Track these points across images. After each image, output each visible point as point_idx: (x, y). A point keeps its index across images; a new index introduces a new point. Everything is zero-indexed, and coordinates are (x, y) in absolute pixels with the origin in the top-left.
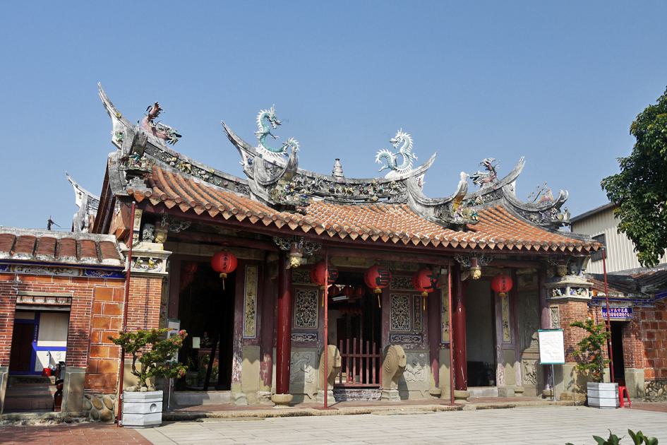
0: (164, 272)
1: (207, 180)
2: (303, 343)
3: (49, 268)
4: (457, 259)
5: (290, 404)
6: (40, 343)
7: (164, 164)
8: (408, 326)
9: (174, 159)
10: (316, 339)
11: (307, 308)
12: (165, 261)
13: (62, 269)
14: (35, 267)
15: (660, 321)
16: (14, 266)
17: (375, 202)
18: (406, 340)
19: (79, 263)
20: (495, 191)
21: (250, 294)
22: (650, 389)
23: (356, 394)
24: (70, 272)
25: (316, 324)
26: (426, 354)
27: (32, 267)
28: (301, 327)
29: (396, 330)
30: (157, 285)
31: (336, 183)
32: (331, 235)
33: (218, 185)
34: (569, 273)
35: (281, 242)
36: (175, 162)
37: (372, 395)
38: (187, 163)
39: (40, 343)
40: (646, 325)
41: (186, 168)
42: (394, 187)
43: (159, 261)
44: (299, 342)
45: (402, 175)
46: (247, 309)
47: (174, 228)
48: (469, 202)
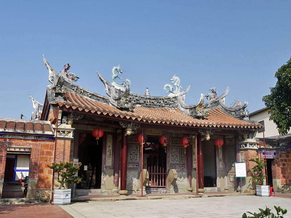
0: (71, 137)
1: (90, 97)
2: (132, 168)
3: (21, 136)
7: (71, 90)
9: (76, 88)
10: (138, 167)
11: (134, 153)
12: (72, 133)
16: (6, 135)
17: (164, 107)
19: (34, 133)
20: (216, 102)
21: (109, 147)
22: (284, 188)
27: (14, 135)
29: (173, 162)
30: (68, 143)
34: (248, 138)
35: (123, 124)
36: (76, 89)
38: (81, 90)
40: (282, 160)
41: (81, 92)
42: (172, 100)
43: (70, 132)
44: (130, 168)
45: (175, 95)
46: (108, 153)
47: (76, 118)
48: (204, 107)
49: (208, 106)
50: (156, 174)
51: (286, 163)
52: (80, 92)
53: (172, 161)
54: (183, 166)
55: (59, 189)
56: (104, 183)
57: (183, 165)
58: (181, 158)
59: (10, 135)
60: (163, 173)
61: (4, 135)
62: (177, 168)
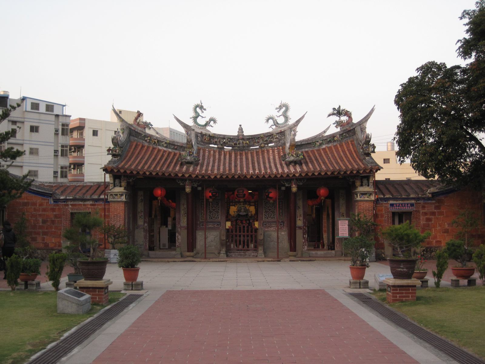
0: (124, 200)
1: (166, 147)
2: (212, 228)
3: (81, 201)
4: (282, 182)
5: (193, 257)
6: (415, 271)
7: (144, 142)
8: (274, 218)
9: (149, 138)
10: (219, 226)
11: (214, 210)
12: (124, 195)
13: (86, 201)
14: (76, 201)
15: (438, 211)
16: (68, 201)
17: (263, 147)
18: (273, 225)
19: (91, 198)
20: (350, 131)
21: (183, 205)
22: (425, 252)
23: (243, 254)
24: (89, 202)
25: (220, 218)
26: (286, 233)
27: (75, 201)
28: (211, 220)
29: (267, 220)
30: (122, 206)
31: (239, 139)
32: (200, 177)
33: (172, 149)
34: (362, 185)
35: (180, 182)
36: (149, 140)
37: (252, 254)
38: (156, 139)
39: (415, 271)
40: (426, 214)
41: (155, 142)
42: (275, 137)
43: (122, 195)
44: (210, 228)
45: (281, 129)
46: (182, 212)
47: (129, 179)
48: (328, 140)
49: (336, 139)
50: (244, 234)
51: (433, 217)
52: (154, 143)
53: (265, 218)
54: (281, 225)
55: (350, 281)
56: (180, 245)
57: (282, 223)
58: (279, 214)
59: (71, 201)
60: (254, 233)
61: (67, 201)
62: (273, 227)
